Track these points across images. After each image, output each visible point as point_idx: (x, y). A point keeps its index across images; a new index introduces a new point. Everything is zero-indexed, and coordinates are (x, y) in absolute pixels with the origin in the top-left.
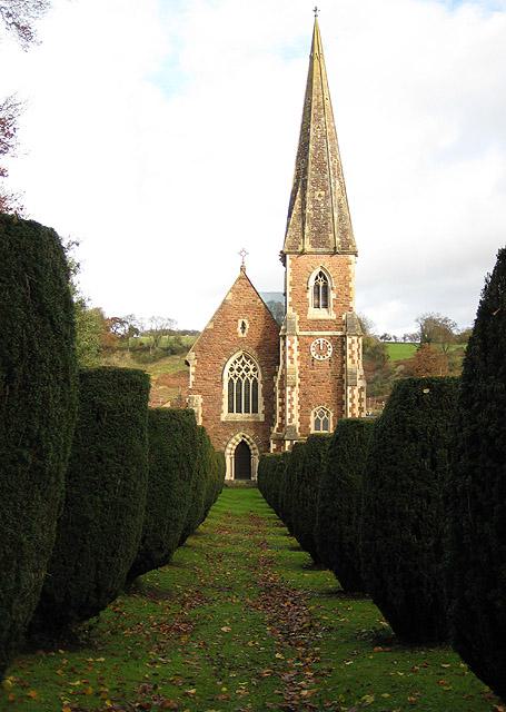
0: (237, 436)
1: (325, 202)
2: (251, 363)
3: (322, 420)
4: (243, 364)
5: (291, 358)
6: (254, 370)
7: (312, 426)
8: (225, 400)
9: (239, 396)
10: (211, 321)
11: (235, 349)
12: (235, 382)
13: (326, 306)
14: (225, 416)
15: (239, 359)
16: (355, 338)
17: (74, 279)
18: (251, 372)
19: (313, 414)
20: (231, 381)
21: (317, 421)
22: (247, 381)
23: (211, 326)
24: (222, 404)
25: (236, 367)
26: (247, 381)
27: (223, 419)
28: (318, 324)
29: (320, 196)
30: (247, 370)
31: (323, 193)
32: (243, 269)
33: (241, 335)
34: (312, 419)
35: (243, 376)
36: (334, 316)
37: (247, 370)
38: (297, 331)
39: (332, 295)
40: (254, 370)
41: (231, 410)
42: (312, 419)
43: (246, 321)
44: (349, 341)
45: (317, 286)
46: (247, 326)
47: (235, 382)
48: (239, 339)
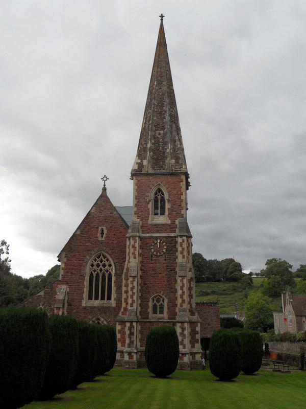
7: (150, 310)
8: (86, 290)
9: (103, 287)
12: (94, 275)
18: (107, 267)
20: (91, 275)
21: (155, 307)
23: (78, 233)
25: (95, 263)
26: (104, 275)
28: (159, 228)
29: (159, 134)
30: (104, 266)
31: (162, 132)
34: (151, 304)
41: (90, 298)
42: (151, 304)
43: (104, 228)
46: (105, 232)
47: (94, 275)
48: (99, 241)
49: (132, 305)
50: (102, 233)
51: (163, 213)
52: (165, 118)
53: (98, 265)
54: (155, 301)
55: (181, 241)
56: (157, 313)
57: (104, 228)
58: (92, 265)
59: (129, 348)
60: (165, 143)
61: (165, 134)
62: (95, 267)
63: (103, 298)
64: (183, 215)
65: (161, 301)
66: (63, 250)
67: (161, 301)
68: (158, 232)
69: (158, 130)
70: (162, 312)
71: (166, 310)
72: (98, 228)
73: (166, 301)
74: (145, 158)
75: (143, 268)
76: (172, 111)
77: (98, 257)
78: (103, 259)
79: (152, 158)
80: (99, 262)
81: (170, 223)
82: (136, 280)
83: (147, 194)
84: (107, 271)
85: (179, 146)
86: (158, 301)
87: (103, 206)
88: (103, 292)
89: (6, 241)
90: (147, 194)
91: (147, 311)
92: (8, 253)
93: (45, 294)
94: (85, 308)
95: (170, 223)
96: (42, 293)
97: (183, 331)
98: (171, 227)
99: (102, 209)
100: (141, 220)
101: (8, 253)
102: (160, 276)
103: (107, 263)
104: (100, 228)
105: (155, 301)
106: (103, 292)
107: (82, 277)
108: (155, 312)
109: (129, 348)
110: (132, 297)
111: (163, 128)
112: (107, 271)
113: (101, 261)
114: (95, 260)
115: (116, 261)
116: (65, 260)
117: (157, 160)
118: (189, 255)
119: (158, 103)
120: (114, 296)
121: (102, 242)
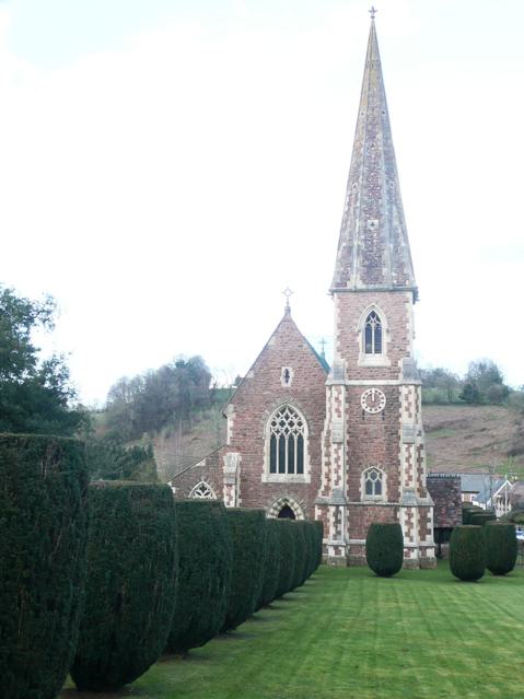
3: (374, 482)
7: (362, 489)
8: (266, 459)
12: (278, 438)
18: (296, 426)
20: (273, 437)
21: (368, 484)
22: (291, 438)
25: (278, 421)
26: (291, 438)
28: (373, 372)
29: (373, 225)
31: (376, 222)
35: (287, 431)
39: (386, 339)
41: (273, 470)
42: (363, 481)
45: (368, 329)
47: (278, 438)
48: (282, 389)
50: (287, 376)
51: (378, 350)
53: (282, 424)
58: (274, 424)
59: (337, 542)
65: (378, 478)
67: (378, 478)
68: (372, 377)
69: (369, 218)
70: (378, 491)
73: (385, 476)
84: (296, 432)
86: (373, 477)
94: (266, 484)
98: (393, 372)
105: (369, 478)
108: (369, 491)
113: (287, 418)
114: (278, 416)
115: (309, 417)
120: (307, 467)
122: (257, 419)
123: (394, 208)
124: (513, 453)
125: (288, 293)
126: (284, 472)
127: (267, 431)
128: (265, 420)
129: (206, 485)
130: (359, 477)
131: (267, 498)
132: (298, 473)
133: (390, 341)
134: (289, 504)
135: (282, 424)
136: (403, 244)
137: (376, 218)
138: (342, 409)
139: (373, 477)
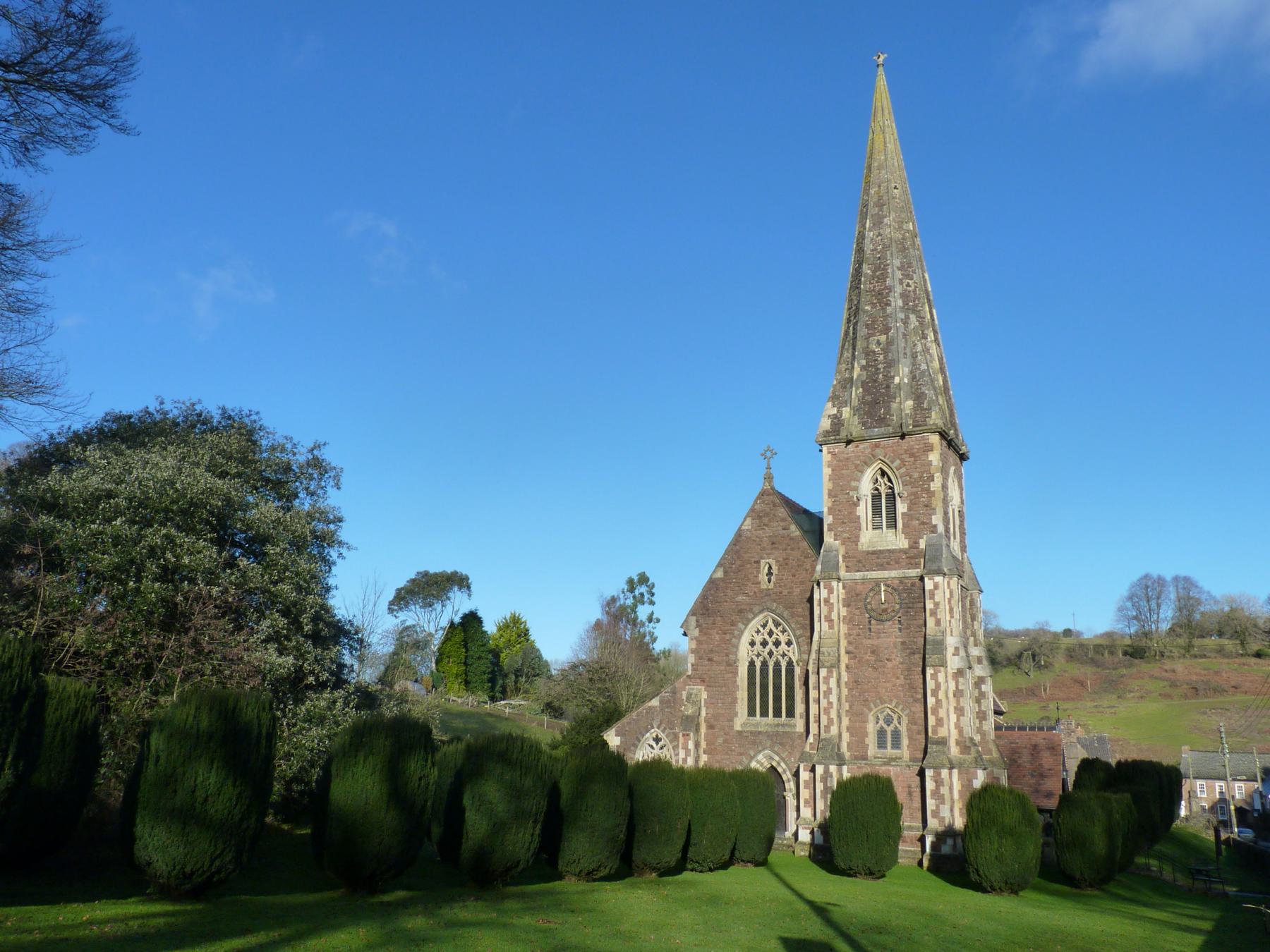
0: (760, 757)
1: (886, 351)
2: (784, 631)
3: (889, 730)
4: (771, 633)
5: (830, 621)
6: (789, 643)
7: (871, 740)
8: (742, 695)
9: (790, 688)
10: (720, 565)
11: (756, 609)
12: (758, 665)
13: (892, 524)
14: (741, 719)
15: (764, 626)
16: (939, 579)
17: (1165, 764)
18: (783, 647)
19: (871, 718)
20: (752, 664)
21: (881, 734)
22: (777, 664)
23: (720, 574)
24: (735, 700)
25: (758, 639)
26: (777, 664)
27: (738, 727)
28: (882, 558)
29: (879, 343)
30: (777, 644)
31: (883, 338)
32: (769, 478)
33: (764, 586)
34: (871, 728)
35: (771, 654)
36: (903, 543)
37: (777, 644)
38: (843, 573)
39: (901, 507)
40: (789, 643)
41: (752, 712)
42: (871, 728)
43: (773, 562)
44: (929, 585)
45: (876, 497)
46: (775, 570)
47: (758, 665)
48: (761, 591)
49: (828, 728)
50: (770, 573)
51: (892, 524)
52: (274, 637)
53: (764, 644)
54: (881, 722)
55: (932, 587)
56: (885, 748)
57: (773, 562)
58: (752, 644)
59: (802, 820)
60: (891, 364)
61: (890, 343)
62: (758, 647)
63: (777, 713)
64: (935, 526)
65: (895, 722)
66: (693, 612)
67: (895, 722)
68: (881, 567)
69: (873, 335)
70: (896, 744)
71: (905, 742)
72: (758, 562)
73: (905, 721)
74: (845, 404)
75: (851, 648)
76: (908, 285)
77: (764, 626)
78: (774, 629)
79: (863, 402)
80: (767, 637)
81: (906, 546)
82: (835, 674)
83: (853, 484)
84: (784, 655)
85: (924, 367)
86: (888, 721)
87: (767, 514)
88: (777, 699)
89: (648, 574)
90: (853, 484)
91: (862, 741)
92: (652, 603)
93: (661, 702)
94: (740, 733)
95: (906, 546)
96: (655, 702)
97: (938, 787)
98: (911, 556)
99: (766, 520)
100: (843, 543)
101: (652, 603)
102: (889, 664)
103: (783, 639)
104: (763, 562)
105: (881, 722)
106: (777, 699)
107: (732, 666)
108: (881, 744)
109: (802, 820)
110: (827, 711)
111: (886, 330)
112: (784, 655)
113: (771, 633)
114: (758, 632)
115: (798, 633)
116: (696, 632)
117: (875, 403)
118: (952, 617)
119: (874, 272)
120: (799, 708)
121: (767, 593)
122: (728, 637)
123: (913, 318)
124: (543, 711)
125: (769, 454)
126: (754, 715)
127: (744, 653)
128: (739, 637)
129: (661, 735)
130: (866, 721)
131: (741, 754)
132: (762, 715)
133: (296, 502)
134: (774, 764)
135: (764, 644)
136: (924, 367)
137: (882, 333)
138: (834, 616)
139: (888, 721)
